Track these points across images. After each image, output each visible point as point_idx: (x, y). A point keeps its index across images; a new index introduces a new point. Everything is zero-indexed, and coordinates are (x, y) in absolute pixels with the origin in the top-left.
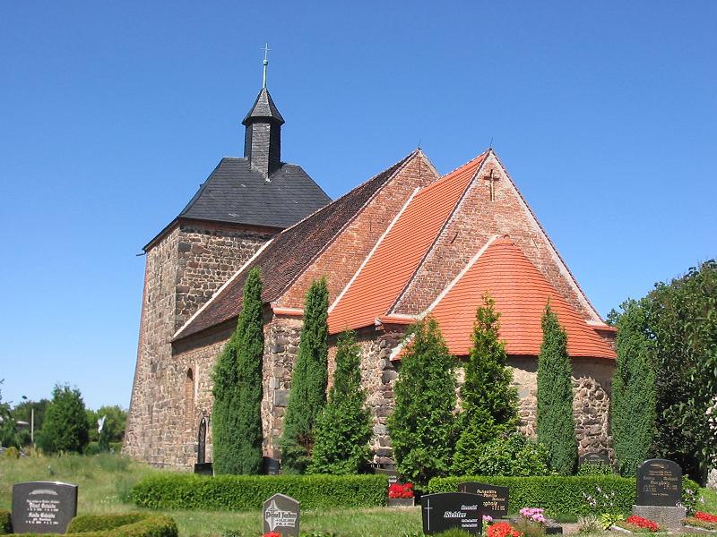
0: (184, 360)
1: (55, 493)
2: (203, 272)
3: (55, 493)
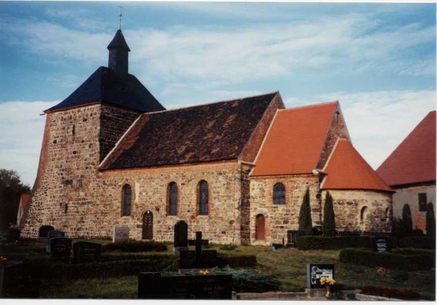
0: (120, 177)
1: (384, 240)
2: (111, 131)
3: (384, 240)
